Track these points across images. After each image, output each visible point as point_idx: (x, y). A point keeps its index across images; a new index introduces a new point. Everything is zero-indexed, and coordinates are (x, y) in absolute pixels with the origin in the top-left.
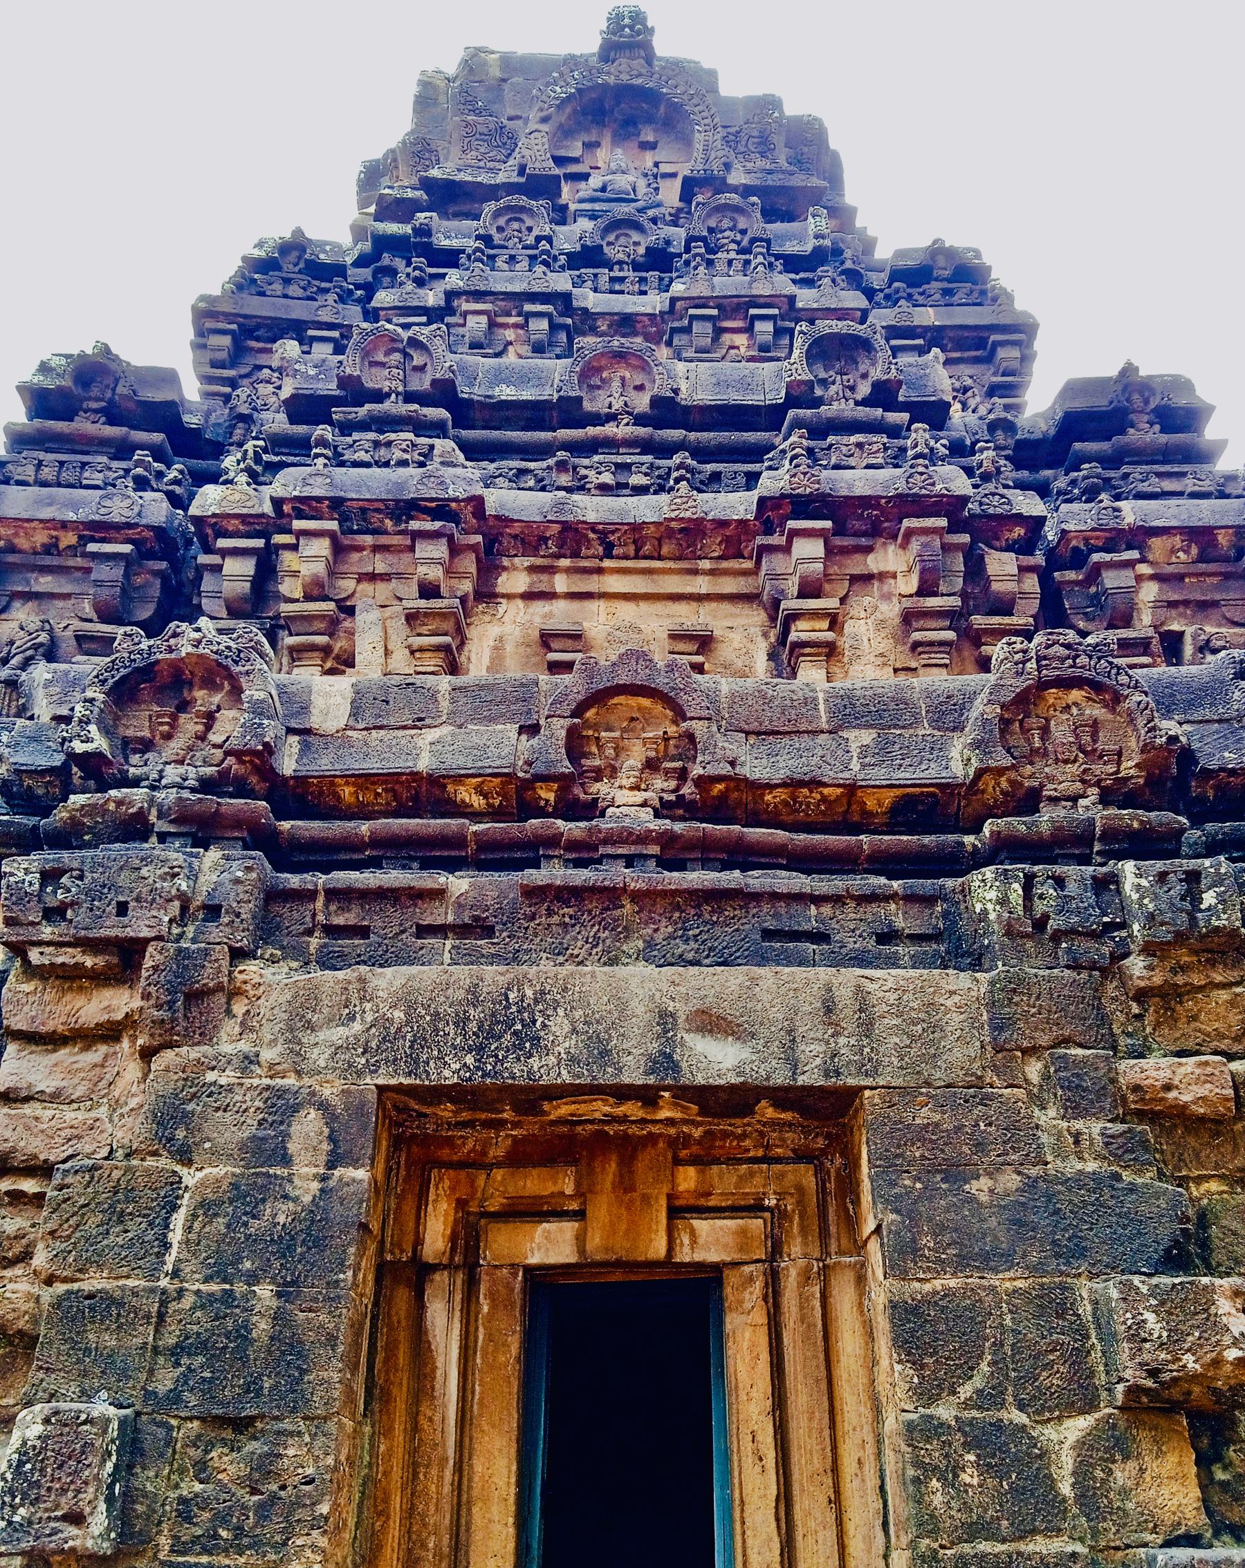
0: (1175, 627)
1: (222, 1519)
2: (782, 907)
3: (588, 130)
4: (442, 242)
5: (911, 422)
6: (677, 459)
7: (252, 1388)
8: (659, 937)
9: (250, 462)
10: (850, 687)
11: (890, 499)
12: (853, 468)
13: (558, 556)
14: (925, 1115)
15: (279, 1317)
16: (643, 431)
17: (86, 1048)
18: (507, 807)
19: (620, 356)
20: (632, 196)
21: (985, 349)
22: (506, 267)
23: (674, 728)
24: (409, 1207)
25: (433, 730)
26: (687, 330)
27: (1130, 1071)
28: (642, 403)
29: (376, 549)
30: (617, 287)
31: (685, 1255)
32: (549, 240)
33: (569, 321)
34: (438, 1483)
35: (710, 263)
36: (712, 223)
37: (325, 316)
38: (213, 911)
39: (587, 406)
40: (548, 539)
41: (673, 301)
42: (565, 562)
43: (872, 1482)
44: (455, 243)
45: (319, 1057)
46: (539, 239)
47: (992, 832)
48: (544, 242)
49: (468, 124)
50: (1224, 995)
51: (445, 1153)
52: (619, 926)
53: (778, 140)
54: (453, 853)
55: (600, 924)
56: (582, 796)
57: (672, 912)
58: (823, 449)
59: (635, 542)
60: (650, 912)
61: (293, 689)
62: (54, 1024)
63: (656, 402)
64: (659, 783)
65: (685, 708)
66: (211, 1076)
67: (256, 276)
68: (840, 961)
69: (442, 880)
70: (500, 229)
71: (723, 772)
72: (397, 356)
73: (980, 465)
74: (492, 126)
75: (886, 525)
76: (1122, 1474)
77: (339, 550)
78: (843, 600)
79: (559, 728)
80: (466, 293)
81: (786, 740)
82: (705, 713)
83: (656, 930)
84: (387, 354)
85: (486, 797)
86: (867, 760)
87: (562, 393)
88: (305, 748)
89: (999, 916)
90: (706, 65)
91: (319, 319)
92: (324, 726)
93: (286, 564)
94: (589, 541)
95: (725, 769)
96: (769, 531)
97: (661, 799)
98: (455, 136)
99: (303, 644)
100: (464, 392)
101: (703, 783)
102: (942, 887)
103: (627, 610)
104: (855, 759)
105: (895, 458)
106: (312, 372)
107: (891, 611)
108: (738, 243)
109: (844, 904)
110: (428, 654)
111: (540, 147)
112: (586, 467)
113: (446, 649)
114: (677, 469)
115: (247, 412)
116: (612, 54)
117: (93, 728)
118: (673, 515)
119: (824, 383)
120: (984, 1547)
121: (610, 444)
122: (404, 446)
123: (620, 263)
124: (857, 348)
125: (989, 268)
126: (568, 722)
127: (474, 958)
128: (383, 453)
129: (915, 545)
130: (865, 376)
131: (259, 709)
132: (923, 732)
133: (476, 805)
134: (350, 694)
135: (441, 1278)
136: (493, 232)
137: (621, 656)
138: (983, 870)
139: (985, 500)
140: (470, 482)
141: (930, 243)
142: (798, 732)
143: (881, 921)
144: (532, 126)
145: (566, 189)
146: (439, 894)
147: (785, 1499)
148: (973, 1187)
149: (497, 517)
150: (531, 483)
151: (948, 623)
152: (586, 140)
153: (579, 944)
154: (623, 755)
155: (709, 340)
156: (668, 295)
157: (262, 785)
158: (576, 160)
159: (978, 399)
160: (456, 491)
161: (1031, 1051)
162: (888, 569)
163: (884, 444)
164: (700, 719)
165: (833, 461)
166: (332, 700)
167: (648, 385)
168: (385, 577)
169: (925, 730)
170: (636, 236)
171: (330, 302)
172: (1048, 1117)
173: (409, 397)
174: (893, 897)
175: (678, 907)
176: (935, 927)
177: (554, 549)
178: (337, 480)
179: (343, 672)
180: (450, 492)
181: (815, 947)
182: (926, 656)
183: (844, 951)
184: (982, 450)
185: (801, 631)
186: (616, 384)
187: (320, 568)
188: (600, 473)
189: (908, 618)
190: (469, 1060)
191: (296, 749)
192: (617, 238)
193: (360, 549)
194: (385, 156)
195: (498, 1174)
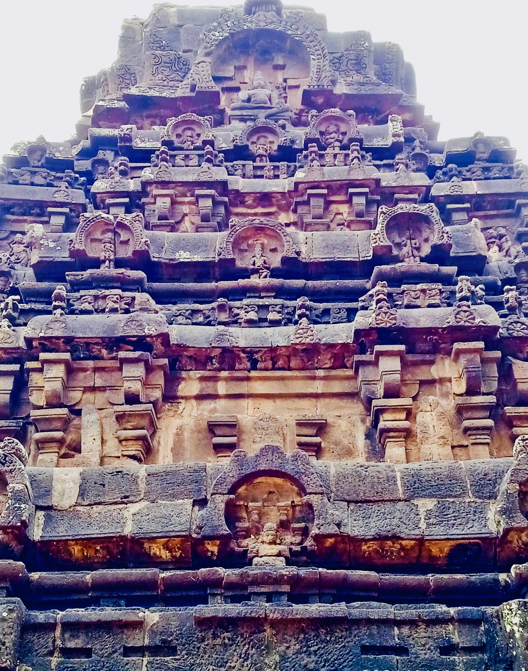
2: (374, 629)
3: (238, 58)
4: (139, 144)
5: (458, 275)
6: (299, 302)
8: (290, 652)
9: (10, 311)
10: (418, 468)
11: (444, 329)
12: (418, 307)
13: (220, 370)
16: (276, 282)
18: (185, 557)
19: (260, 230)
20: (269, 105)
21: (513, 208)
22: (182, 163)
23: (299, 499)
25: (135, 504)
26: (307, 203)
28: (276, 261)
29: (96, 370)
30: (259, 173)
32: (211, 143)
33: (226, 199)
35: (322, 156)
36: (323, 128)
37: (59, 198)
39: (239, 264)
40: (213, 358)
41: (297, 184)
42: (224, 374)
44: (148, 145)
46: (205, 143)
47: (516, 574)
48: (208, 146)
49: (156, 56)
52: (262, 645)
53: (369, 61)
54: (148, 593)
55: (249, 644)
56: (237, 549)
57: (299, 634)
58: (398, 294)
59: (272, 359)
60: (283, 634)
61: (40, 477)
63: (285, 260)
64: (289, 538)
65: (306, 486)
67: (12, 170)
69: (141, 614)
70: (178, 136)
71: (333, 532)
72: (110, 235)
73: (507, 301)
74: (172, 57)
75: (443, 346)
77: (70, 371)
78: (414, 398)
80: (156, 182)
81: (375, 507)
82: (319, 490)
83: (288, 648)
84: (103, 233)
85: (170, 551)
86: (431, 521)
87: (221, 257)
88: (48, 519)
89: (522, 636)
90: (318, 11)
91: (56, 200)
92: (61, 504)
93: (34, 382)
94: (240, 358)
95: (333, 529)
96: (363, 352)
97: (291, 549)
98: (147, 64)
99: (42, 439)
100: (155, 256)
101: (318, 538)
102: (484, 613)
103: (267, 406)
104: (423, 520)
105: (448, 298)
106: (52, 245)
108: (341, 142)
109: (418, 626)
110: (131, 443)
111: (205, 73)
112: (238, 308)
113: (143, 438)
114: (300, 309)
115: (7, 270)
116: (253, 9)
118: (297, 341)
119: (399, 246)
121: (254, 291)
122: (115, 299)
123: (261, 156)
124: (421, 222)
125: (515, 152)
126: (226, 497)
128: (100, 304)
129: (463, 360)
130: (426, 240)
131: (18, 497)
132: (468, 500)
133: (164, 556)
134: (79, 481)
136: (174, 138)
137: (262, 450)
138: (510, 602)
139: (510, 326)
140: (159, 324)
141: (472, 135)
142: (383, 500)
143: (443, 638)
144: (199, 58)
145: (223, 98)
146: (138, 625)
149: (178, 345)
150: (201, 319)
151: (488, 414)
152: (237, 65)
153: (235, 658)
154: (264, 519)
155: (322, 210)
156: (293, 179)
157: (19, 547)
158: (230, 79)
159: (510, 243)
160: (150, 330)
162: (445, 376)
163: (440, 290)
164: (316, 494)
165: (406, 302)
166: (67, 485)
167: (279, 248)
168: (102, 389)
169: (470, 498)
170: (271, 138)
171: (63, 188)
173: (119, 263)
174: (451, 620)
175: (303, 631)
176: (480, 642)
177: (217, 365)
178: (70, 326)
179: (73, 456)
180: (146, 331)
181: (398, 657)
182: (474, 437)
183: (418, 660)
184: (508, 291)
186: (258, 248)
187: (57, 385)
188: (247, 312)
189: (461, 410)
191: (42, 522)
192: (258, 139)
193: (84, 370)
194: (99, 77)
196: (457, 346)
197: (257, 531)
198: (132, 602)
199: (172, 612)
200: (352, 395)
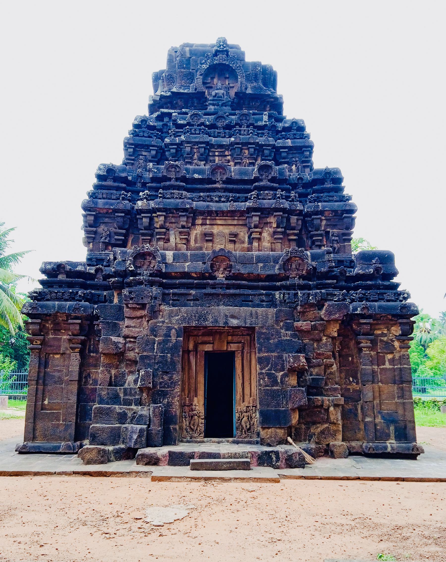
0: (328, 230)
1: (166, 384)
7: (168, 368)
13: (207, 216)
14: (265, 331)
15: (171, 359)
17: (138, 319)
24: (187, 342)
27: (296, 324)
31: (229, 349)
34: (193, 381)
38: (156, 298)
42: (209, 218)
43: (255, 381)
45: (174, 322)
50: (312, 312)
51: (192, 334)
62: (133, 316)
64: (226, 273)
66: (158, 324)
68: (254, 306)
70: (192, 119)
76: (287, 379)
77: (166, 217)
79: (209, 263)
103: (221, 228)
107: (271, 230)
108: (247, 123)
117: (132, 265)
120: (267, 388)
123: (220, 127)
127: (196, 305)
134: (173, 256)
135: (192, 353)
146: (190, 294)
147: (243, 383)
148: (270, 341)
161: (282, 321)
168: (175, 223)
172: (283, 331)
173: (177, 179)
184: (292, 193)
185: (254, 236)
186: (219, 174)
187: (163, 223)
190: (197, 322)
193: (169, 217)
195: (200, 337)
196: (275, 214)
197: (218, 270)
198: (188, 288)
199: (199, 291)
200: (245, 225)
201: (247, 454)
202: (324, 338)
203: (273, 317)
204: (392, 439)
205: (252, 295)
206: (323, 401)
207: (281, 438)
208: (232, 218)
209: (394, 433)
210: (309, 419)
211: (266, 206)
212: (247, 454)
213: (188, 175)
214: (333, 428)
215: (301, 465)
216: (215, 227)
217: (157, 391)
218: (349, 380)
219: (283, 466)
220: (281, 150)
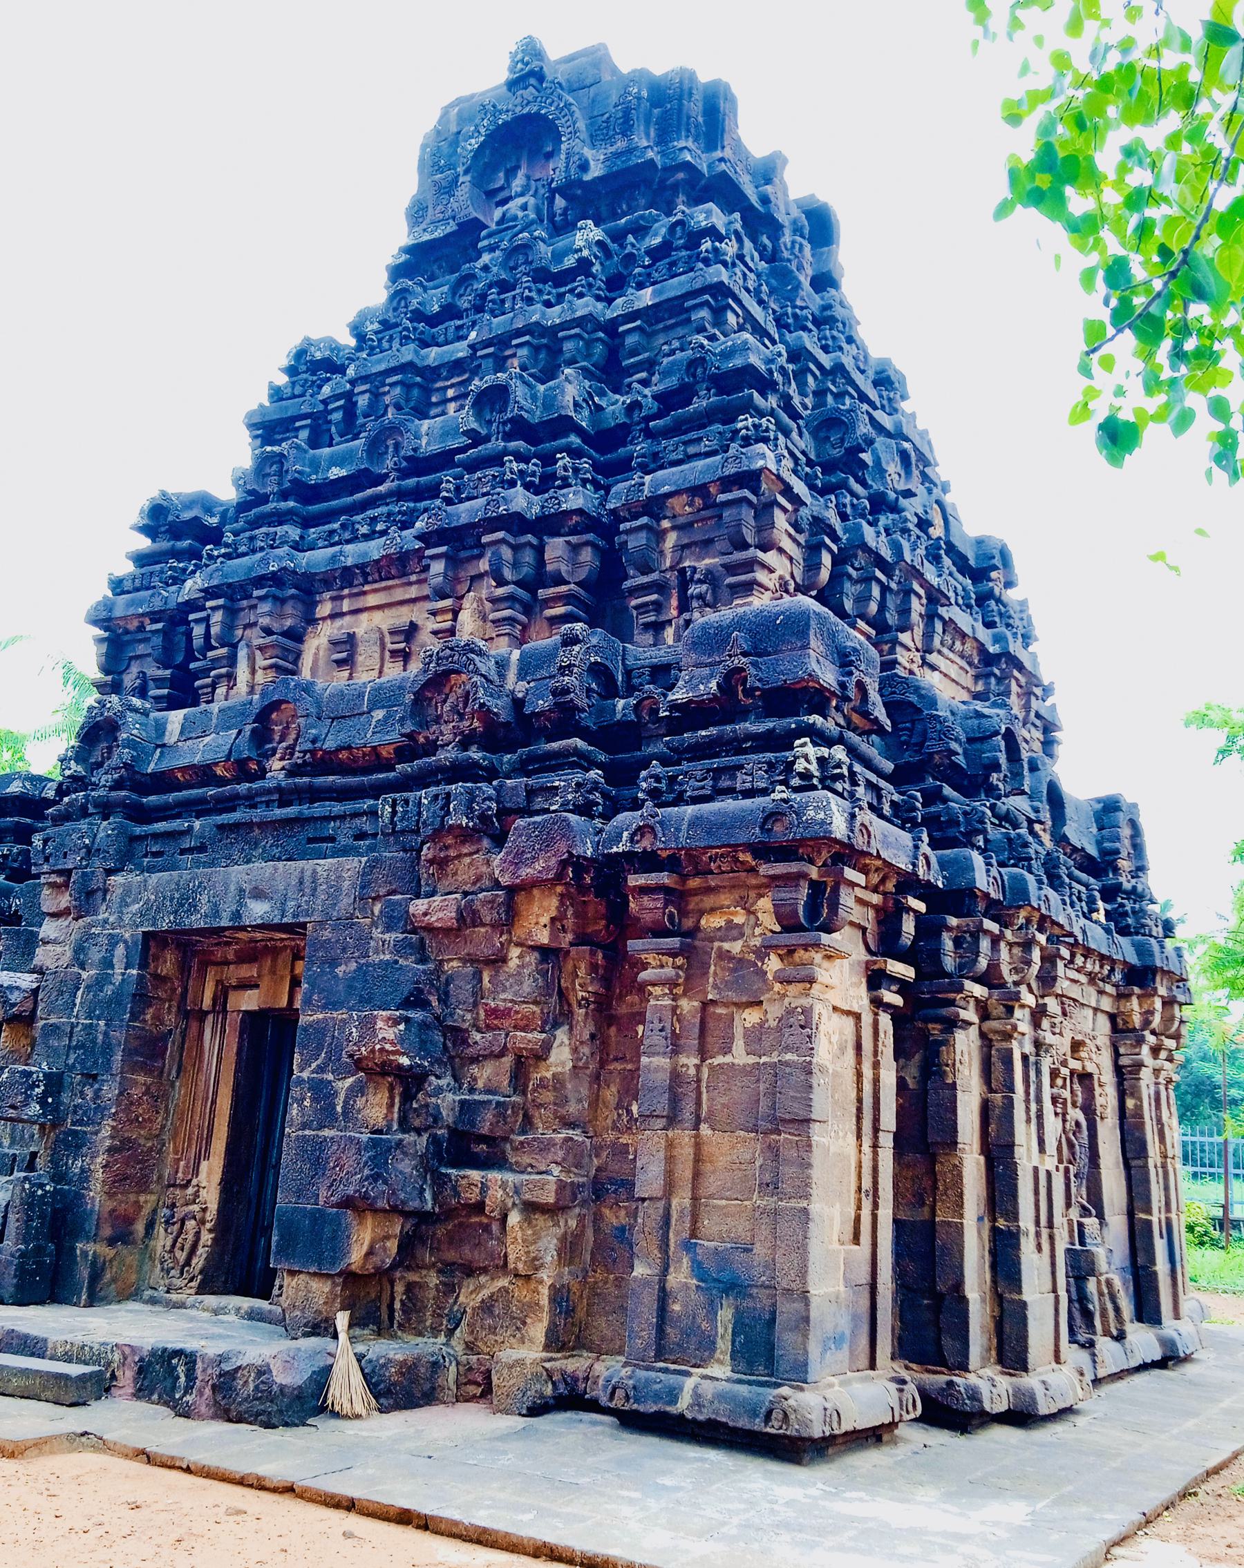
13: (342, 588)
15: (106, 1034)
41: (472, 347)
42: (346, 591)
50: (467, 860)
66: (93, 930)
120: (307, 1132)
123: (466, 310)
127: (197, 864)
172: (376, 933)
193: (243, 609)
201: (112, 1351)
202: (515, 952)
203: (353, 886)
204: (721, 1362)
205: (334, 818)
206: (484, 1188)
207: (318, 1312)
208: (404, 580)
209: (729, 1337)
210: (451, 1255)
211: (464, 520)
212: (112, 1351)
213: (314, 477)
214: (521, 1293)
215: (258, 1414)
216: (364, 617)
217: (64, 1133)
218: (629, 1112)
219: (203, 1409)
220: (621, 329)
